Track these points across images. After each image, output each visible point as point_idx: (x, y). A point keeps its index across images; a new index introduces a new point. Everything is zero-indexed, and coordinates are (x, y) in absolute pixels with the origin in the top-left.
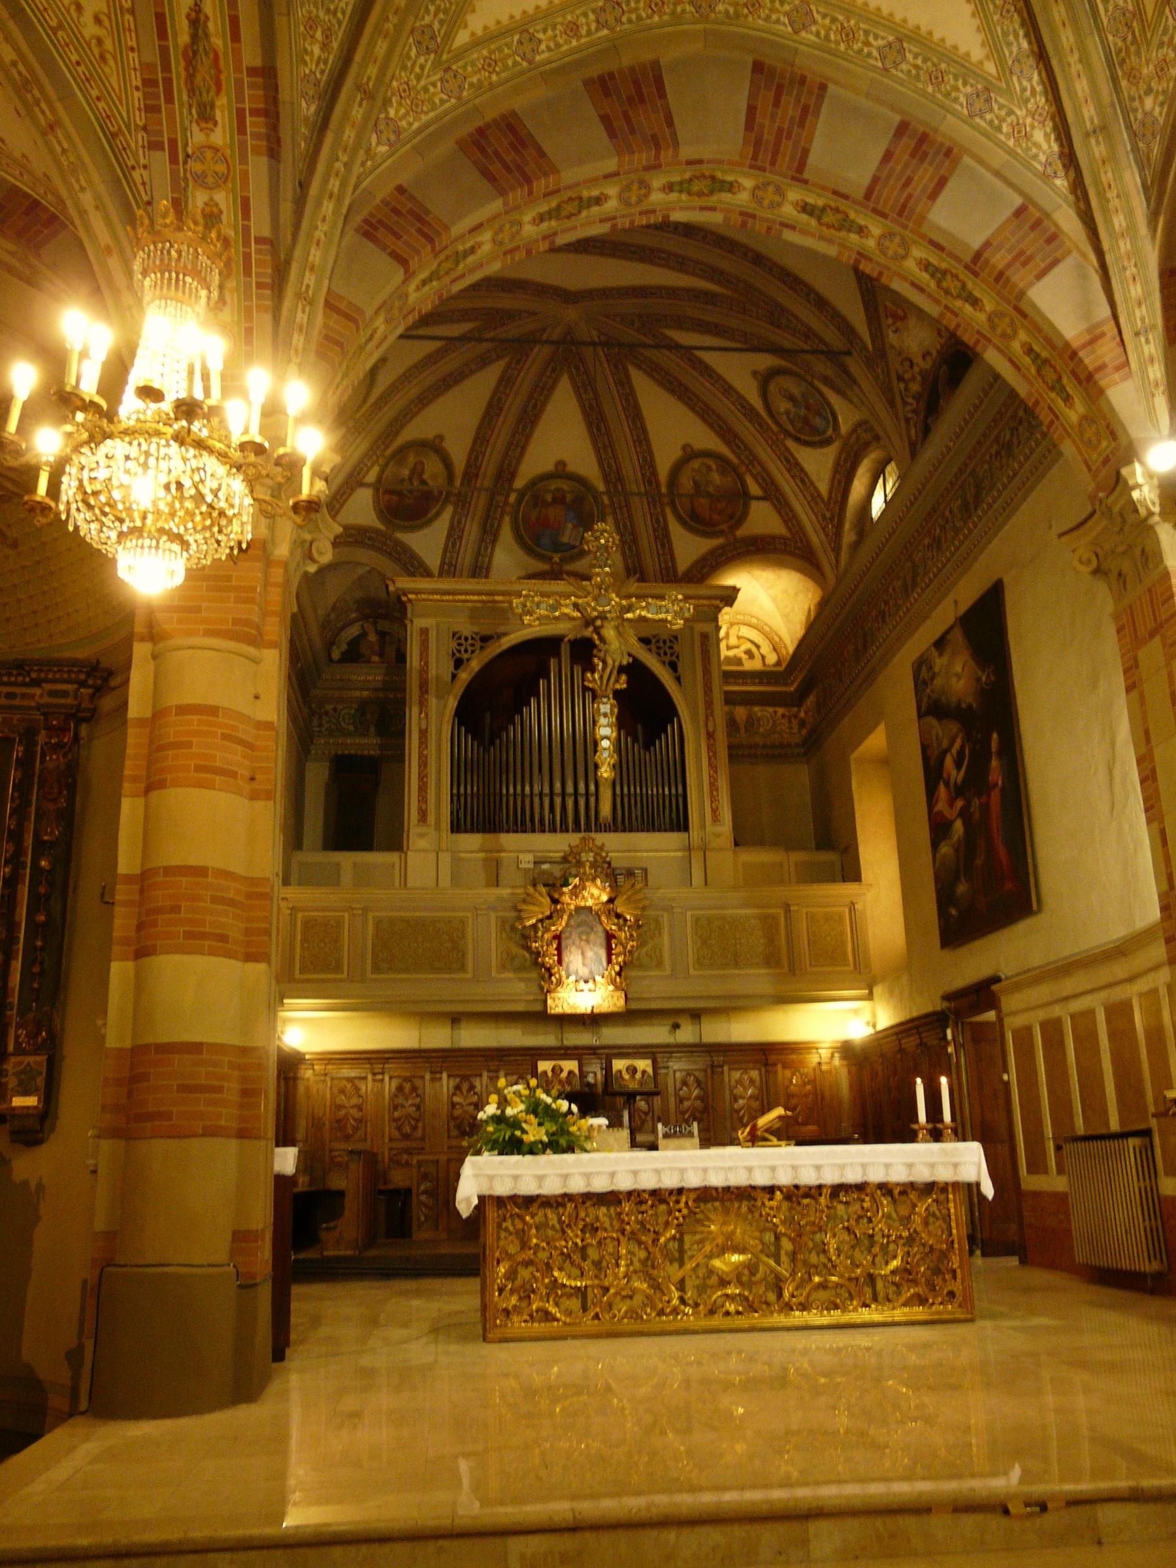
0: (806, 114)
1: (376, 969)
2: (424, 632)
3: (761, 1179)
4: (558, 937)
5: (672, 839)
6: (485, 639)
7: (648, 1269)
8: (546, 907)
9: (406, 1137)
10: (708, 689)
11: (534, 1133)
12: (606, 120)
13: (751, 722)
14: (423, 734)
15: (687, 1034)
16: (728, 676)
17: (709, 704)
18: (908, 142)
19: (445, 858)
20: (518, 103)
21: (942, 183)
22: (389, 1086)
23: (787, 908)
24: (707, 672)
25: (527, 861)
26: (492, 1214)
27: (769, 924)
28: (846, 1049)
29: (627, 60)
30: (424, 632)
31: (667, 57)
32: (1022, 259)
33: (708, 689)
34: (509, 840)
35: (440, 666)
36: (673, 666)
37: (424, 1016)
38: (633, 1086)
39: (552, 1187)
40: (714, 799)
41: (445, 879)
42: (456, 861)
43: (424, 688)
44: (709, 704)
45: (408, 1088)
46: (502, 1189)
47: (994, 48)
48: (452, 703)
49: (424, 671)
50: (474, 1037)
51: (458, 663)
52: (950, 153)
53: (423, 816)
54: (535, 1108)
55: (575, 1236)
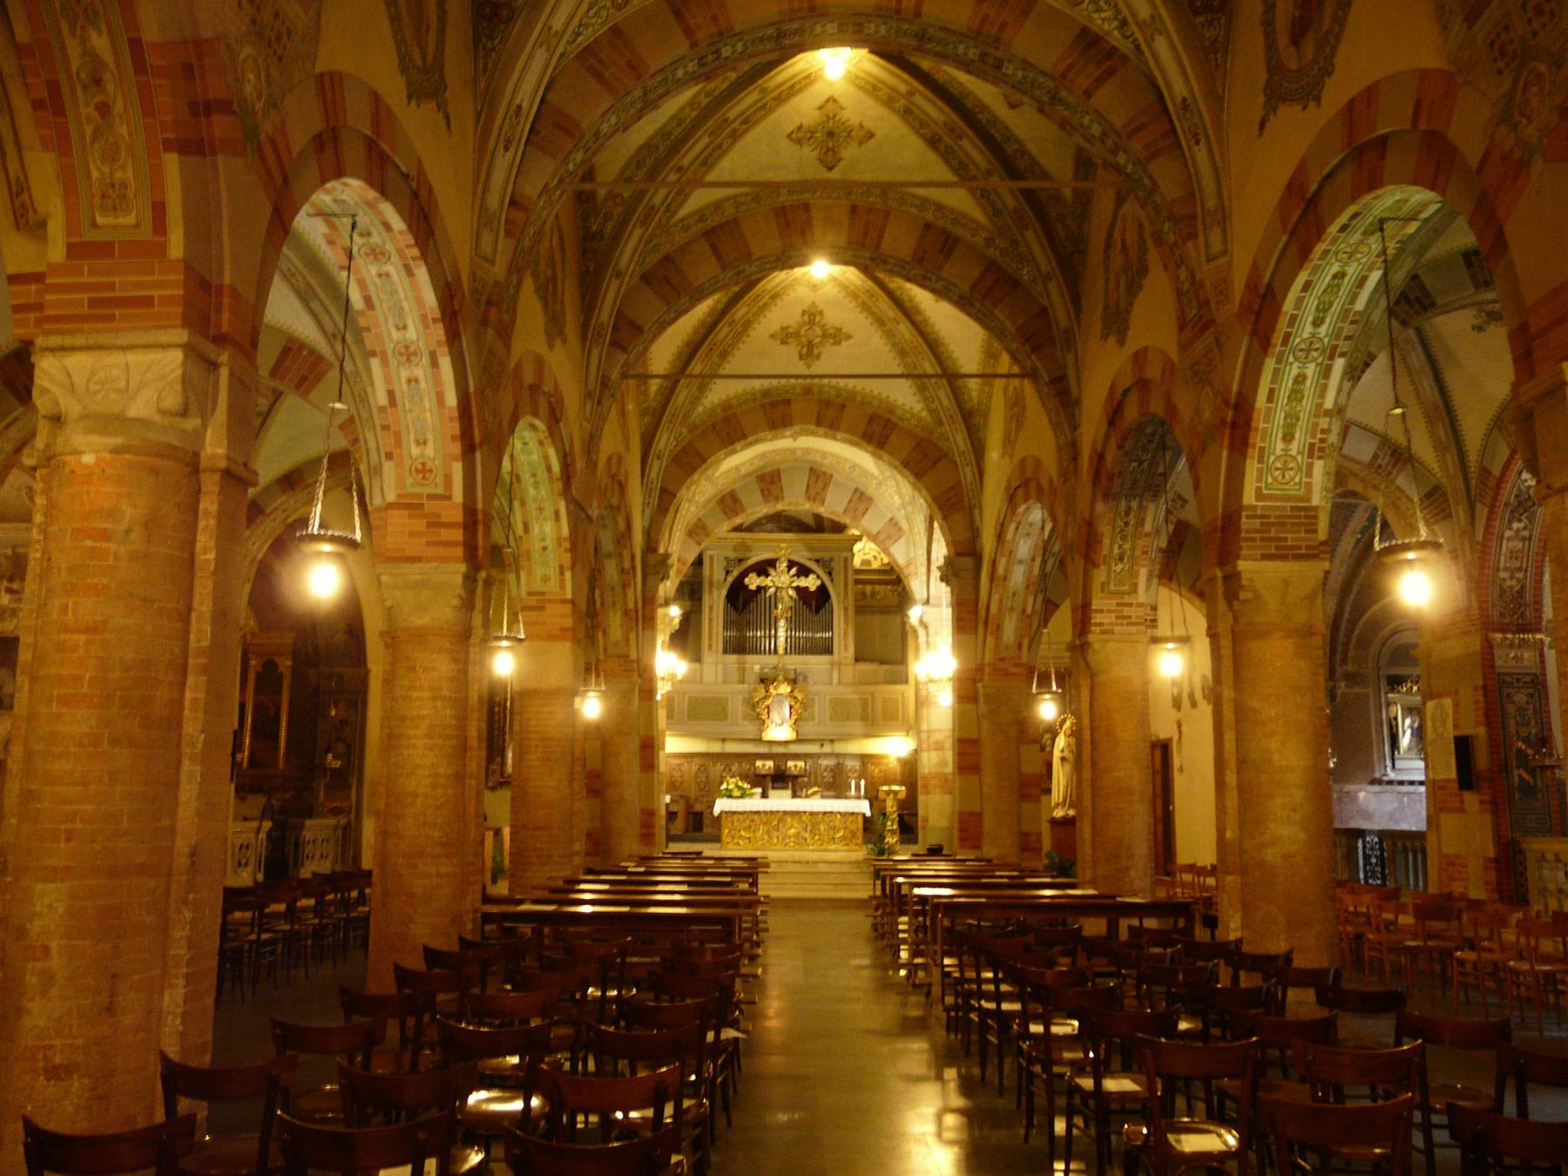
0: (825, 486)
1: (689, 717)
2: (711, 558)
3: (801, 809)
4: (768, 707)
5: (824, 658)
6: (740, 560)
7: (768, 832)
8: (762, 693)
9: (701, 790)
10: (846, 577)
11: (736, 793)
12: (762, 491)
13: (873, 594)
14: (711, 608)
15: (827, 749)
16: (858, 571)
17: (846, 585)
18: (858, 495)
19: (720, 667)
20: (735, 487)
21: (867, 509)
22: (695, 768)
23: (872, 694)
24: (846, 568)
25: (757, 668)
26: (724, 816)
27: (864, 703)
28: (899, 760)
29: (769, 469)
30: (711, 558)
31: (782, 467)
32: (889, 537)
33: (846, 577)
34: (749, 658)
35: (719, 575)
36: (830, 574)
37: (709, 737)
38: (796, 773)
39: (741, 809)
40: (845, 640)
41: (720, 679)
42: (725, 669)
43: (711, 585)
44: (846, 585)
45: (703, 769)
46: (727, 809)
47: (882, 473)
48: (724, 593)
49: (711, 576)
50: (731, 748)
51: (728, 573)
52: (870, 499)
53: (710, 646)
54: (737, 786)
55: (747, 822)
